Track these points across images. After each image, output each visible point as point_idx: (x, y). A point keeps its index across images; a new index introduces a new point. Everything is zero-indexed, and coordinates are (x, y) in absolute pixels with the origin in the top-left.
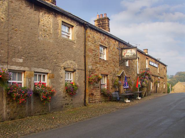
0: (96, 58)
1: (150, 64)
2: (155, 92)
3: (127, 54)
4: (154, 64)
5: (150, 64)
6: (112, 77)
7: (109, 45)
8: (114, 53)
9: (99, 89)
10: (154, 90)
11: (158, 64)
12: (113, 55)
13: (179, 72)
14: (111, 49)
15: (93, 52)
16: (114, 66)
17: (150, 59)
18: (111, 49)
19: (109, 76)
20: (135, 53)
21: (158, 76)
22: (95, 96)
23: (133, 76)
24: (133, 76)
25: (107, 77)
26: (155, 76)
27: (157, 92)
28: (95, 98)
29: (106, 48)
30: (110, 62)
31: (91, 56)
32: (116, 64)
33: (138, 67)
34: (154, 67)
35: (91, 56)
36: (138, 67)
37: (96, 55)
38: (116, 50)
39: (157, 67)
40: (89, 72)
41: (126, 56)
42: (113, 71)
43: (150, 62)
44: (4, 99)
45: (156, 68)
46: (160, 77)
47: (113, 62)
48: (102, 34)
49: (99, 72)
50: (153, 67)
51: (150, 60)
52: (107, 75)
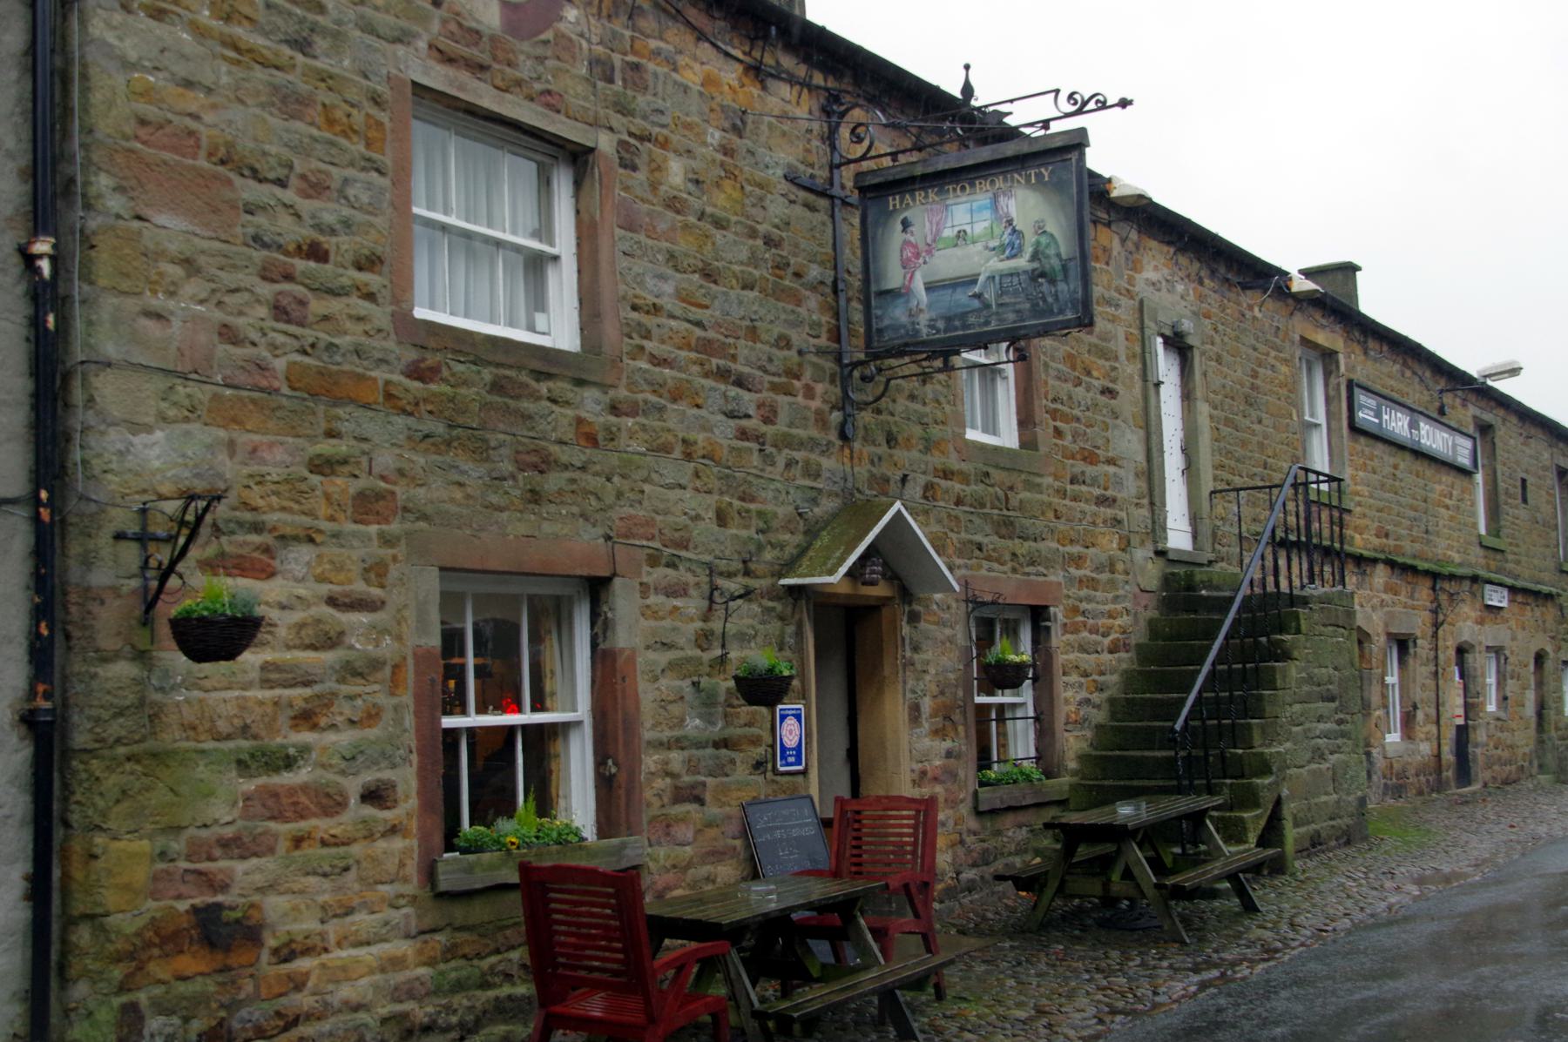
0: (318, 306)
1: (1356, 430)
2: (1449, 774)
3: (947, 263)
4: (1425, 427)
5: (1365, 416)
6: (693, 605)
7: (624, 110)
8: (733, 250)
9: (393, 830)
10: (1426, 748)
11: (1485, 429)
12: (709, 274)
13: (1088, 145)
14: (676, 172)
15: (250, 191)
16: (743, 435)
17: (1353, 361)
18: (676, 172)
19: (624, 602)
20: (1063, 244)
21: (1475, 579)
22: (286, 953)
23: (1092, 584)
24: (1092, 584)
25: (595, 616)
26: (1435, 576)
27: (1481, 774)
28: (298, 982)
29: (578, 158)
30: (657, 387)
31: (189, 264)
32: (783, 417)
33: (1173, 463)
34: (1419, 466)
35: (189, 264)
36: (1173, 463)
37: (316, 253)
38: (777, 208)
39: (1464, 460)
40: (143, 538)
41: (930, 288)
42: (722, 518)
43: (1362, 398)
44: (1380, 630)
45: (1447, 478)
46: (1513, 590)
47: (722, 375)
48: (1385, 348)
49: (387, 541)
50: (1405, 462)
51: (1359, 376)
52: (597, 588)
